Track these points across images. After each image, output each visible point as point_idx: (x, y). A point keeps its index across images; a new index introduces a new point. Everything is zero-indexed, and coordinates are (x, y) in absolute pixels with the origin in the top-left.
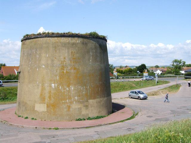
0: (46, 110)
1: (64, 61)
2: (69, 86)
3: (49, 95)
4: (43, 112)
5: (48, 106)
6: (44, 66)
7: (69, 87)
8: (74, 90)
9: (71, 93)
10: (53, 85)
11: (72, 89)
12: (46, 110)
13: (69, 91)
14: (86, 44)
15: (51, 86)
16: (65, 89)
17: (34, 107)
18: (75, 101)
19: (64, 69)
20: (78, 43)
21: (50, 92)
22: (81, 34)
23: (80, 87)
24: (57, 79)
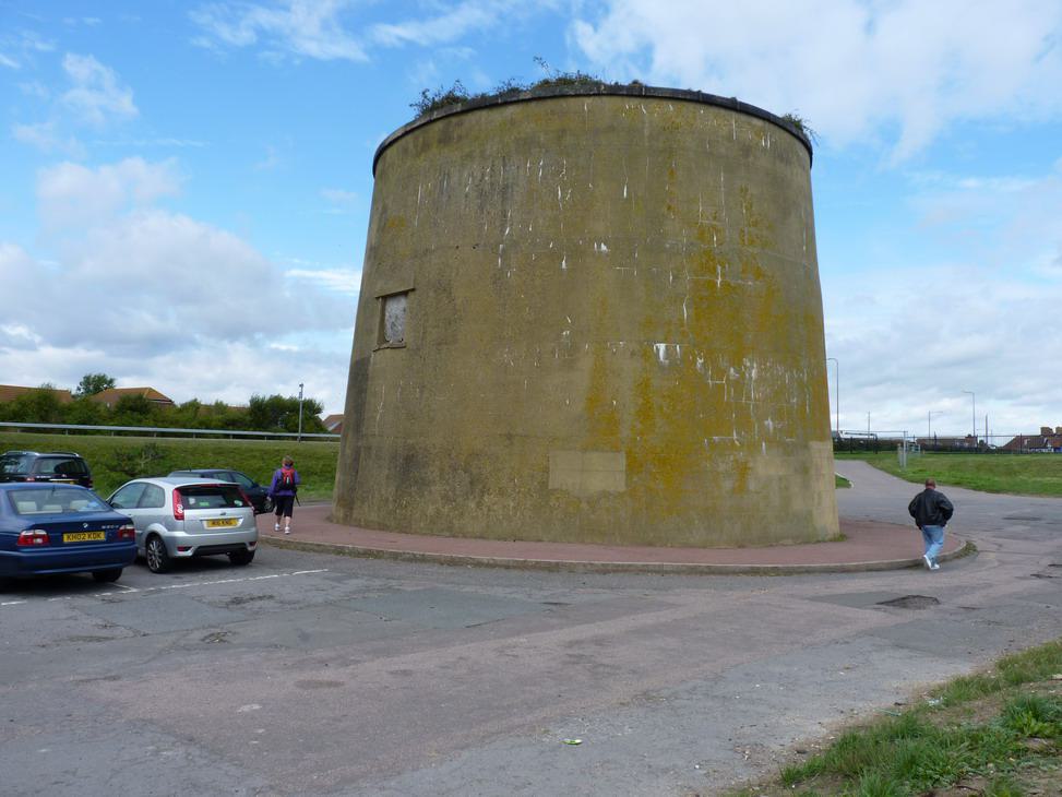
0: (622, 489)
1: (714, 228)
2: (737, 361)
3: (641, 401)
4: (605, 494)
5: (633, 467)
6: (604, 247)
7: (740, 363)
8: (760, 379)
9: (749, 398)
10: (662, 347)
11: (750, 374)
12: (622, 489)
13: (740, 384)
14: (406, 151)
15: (648, 355)
16: (721, 373)
17: (546, 470)
18: (770, 442)
19: (715, 269)
20: (765, 149)
21: (644, 387)
22: (741, 103)
23: (780, 369)
24: (682, 320)
